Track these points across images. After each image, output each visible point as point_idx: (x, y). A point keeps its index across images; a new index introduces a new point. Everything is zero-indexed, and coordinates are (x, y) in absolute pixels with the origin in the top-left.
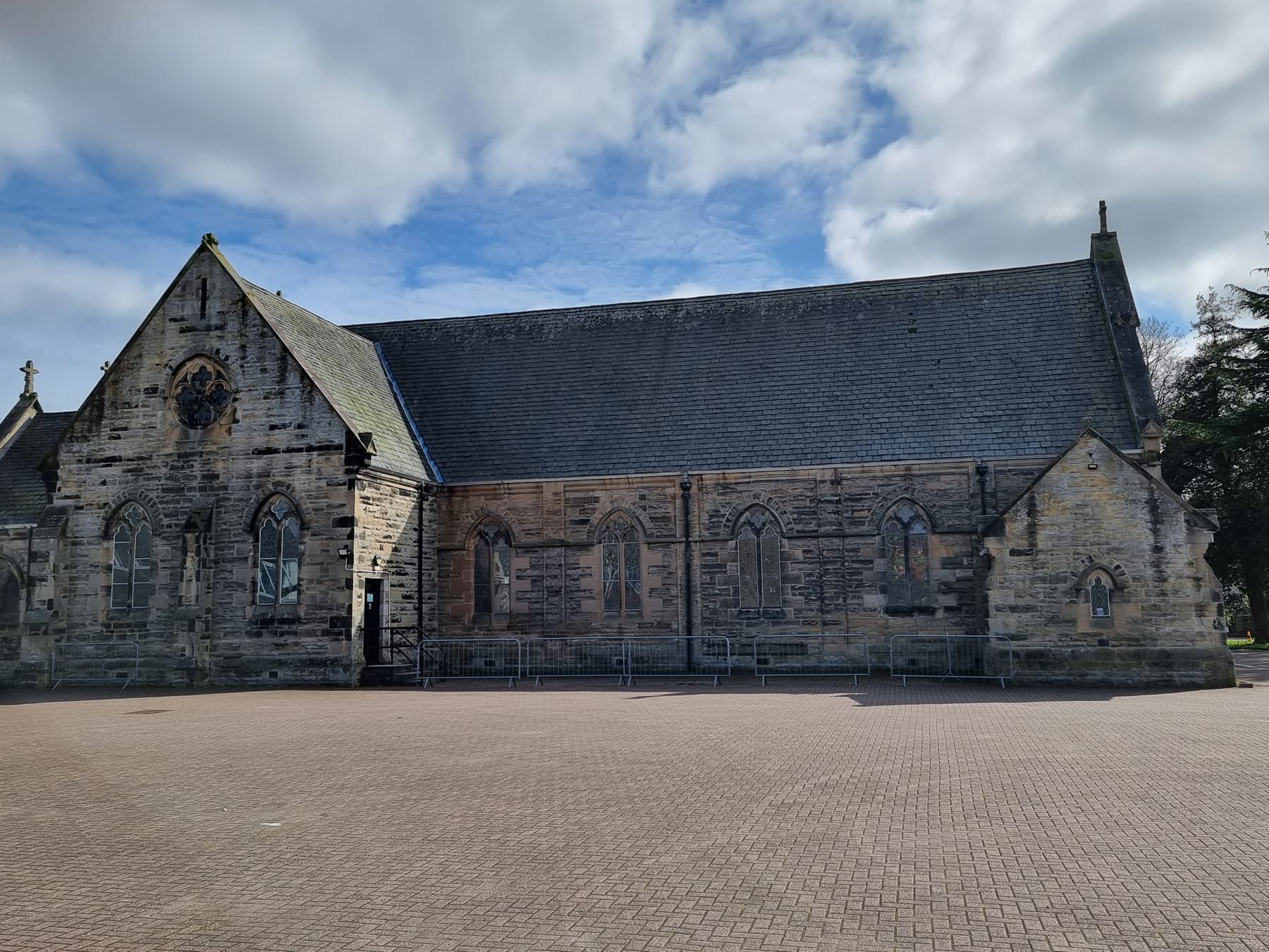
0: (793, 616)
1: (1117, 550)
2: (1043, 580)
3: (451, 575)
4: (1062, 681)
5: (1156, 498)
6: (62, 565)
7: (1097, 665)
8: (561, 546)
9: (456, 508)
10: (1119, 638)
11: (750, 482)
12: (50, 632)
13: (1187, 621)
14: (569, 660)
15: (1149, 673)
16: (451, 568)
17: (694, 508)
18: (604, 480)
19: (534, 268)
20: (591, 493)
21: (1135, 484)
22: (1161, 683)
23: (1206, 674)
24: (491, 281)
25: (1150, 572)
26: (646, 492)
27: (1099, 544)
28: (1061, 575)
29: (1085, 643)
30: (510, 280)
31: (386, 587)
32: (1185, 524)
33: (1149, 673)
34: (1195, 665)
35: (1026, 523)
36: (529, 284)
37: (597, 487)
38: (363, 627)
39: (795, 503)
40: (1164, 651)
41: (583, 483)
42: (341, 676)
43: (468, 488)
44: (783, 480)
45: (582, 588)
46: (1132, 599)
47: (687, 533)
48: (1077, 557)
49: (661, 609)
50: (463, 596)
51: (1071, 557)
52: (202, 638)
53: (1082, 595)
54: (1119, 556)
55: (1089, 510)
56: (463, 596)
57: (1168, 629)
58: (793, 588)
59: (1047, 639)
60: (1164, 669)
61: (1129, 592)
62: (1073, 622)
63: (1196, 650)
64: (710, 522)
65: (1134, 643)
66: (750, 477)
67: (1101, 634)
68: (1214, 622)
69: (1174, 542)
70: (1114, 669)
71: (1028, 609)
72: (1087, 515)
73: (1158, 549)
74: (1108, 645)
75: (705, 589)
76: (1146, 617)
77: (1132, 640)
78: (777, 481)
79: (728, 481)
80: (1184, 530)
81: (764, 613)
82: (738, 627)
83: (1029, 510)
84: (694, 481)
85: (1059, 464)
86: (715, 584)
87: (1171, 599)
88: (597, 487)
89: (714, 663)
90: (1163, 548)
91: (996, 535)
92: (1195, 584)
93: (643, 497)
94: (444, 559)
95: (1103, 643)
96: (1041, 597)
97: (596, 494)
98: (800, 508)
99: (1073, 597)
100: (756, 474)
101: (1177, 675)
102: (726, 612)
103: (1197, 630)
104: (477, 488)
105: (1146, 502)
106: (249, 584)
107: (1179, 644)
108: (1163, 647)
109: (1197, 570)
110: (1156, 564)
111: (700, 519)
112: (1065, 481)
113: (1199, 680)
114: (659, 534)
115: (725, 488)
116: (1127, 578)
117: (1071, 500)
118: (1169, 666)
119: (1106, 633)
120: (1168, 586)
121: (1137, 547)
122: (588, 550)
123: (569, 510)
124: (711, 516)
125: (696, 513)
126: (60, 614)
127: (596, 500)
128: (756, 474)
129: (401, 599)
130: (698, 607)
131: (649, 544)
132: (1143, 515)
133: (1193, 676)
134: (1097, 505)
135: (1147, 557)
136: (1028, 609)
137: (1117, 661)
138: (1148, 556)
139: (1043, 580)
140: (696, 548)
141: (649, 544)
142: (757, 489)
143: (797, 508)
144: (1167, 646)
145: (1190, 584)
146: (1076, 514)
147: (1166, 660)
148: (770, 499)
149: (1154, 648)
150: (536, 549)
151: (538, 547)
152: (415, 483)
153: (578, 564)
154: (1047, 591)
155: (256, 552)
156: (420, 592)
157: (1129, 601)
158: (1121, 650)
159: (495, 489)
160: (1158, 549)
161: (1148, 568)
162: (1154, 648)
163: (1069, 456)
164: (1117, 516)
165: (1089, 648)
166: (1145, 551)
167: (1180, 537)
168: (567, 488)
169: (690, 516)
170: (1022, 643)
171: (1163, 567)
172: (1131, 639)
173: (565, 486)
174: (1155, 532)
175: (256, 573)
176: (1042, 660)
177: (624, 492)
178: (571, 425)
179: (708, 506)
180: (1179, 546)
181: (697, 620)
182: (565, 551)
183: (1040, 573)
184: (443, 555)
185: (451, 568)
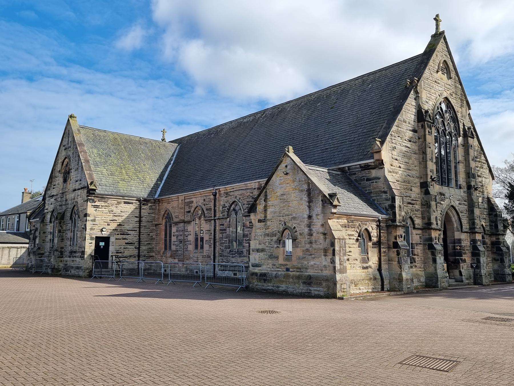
0: (245, 253)
1: (294, 218)
2: (268, 235)
3: (158, 235)
4: (270, 290)
5: (311, 188)
6: (42, 232)
7: (283, 281)
8: (183, 222)
9: (160, 208)
10: (294, 267)
11: (233, 191)
12: (36, 254)
13: (320, 259)
14: (183, 272)
15: (301, 288)
16: (159, 232)
17: (217, 204)
18: (194, 193)
19: (510, 90)
20: (191, 199)
21: (302, 181)
22: (306, 294)
23: (325, 290)
24: (487, 100)
25: (306, 230)
26: (205, 198)
27: (288, 215)
28: (274, 232)
29: (281, 269)
30: (498, 98)
31: (112, 239)
32: (321, 202)
33: (301, 288)
34: (320, 284)
35: (264, 205)
36: (508, 98)
37: (193, 197)
38: (93, 255)
39: (247, 199)
40: (310, 275)
41: (189, 195)
42: (81, 273)
43: (163, 199)
44: (243, 189)
45: (188, 240)
46: (300, 245)
47: (215, 216)
48: (280, 222)
49: (208, 249)
50: (161, 243)
51: (278, 222)
52: (58, 257)
53: (281, 243)
54: (295, 222)
55: (285, 197)
56: (161, 243)
57: (312, 263)
58: (246, 240)
59: (268, 267)
60: (308, 286)
61: (298, 242)
62: (277, 258)
63: (322, 275)
64: (223, 210)
65: (299, 270)
66: (233, 188)
67: (287, 265)
68: (331, 259)
69: (316, 213)
70: (289, 285)
71: (263, 250)
72: (285, 199)
73: (310, 217)
74: (289, 271)
75: (220, 240)
76: (304, 256)
77: (299, 269)
78: (242, 190)
79: (228, 191)
80: (321, 205)
81: (237, 252)
82: (229, 258)
83: (265, 198)
84: (217, 192)
85: (276, 173)
86: (223, 238)
87: (314, 246)
88: (193, 197)
89: (221, 274)
90: (312, 216)
91: (254, 212)
92: (324, 236)
93: (204, 200)
94: (157, 228)
95: (288, 270)
96: (267, 244)
97: (191, 200)
98: (249, 202)
99: (278, 244)
100: (235, 187)
101: (314, 289)
102: (226, 251)
103: (324, 264)
104: (165, 199)
105: (306, 191)
106: (70, 238)
107: (316, 271)
108: (310, 273)
109: (325, 229)
110: (309, 226)
111: (219, 208)
112: (278, 182)
113: (322, 294)
114: (208, 216)
115: (227, 194)
116: (298, 234)
117: (279, 192)
118: (310, 284)
119: (289, 264)
120: (313, 238)
121: (302, 216)
122: (190, 224)
123: (186, 207)
124: (223, 207)
125: (218, 206)
126: (41, 248)
127: (192, 202)
128: (235, 187)
129: (125, 244)
130: (217, 249)
131: (206, 220)
132: (305, 198)
133: (319, 291)
134: (289, 194)
135: (306, 222)
136: (263, 250)
137: (291, 280)
138: (306, 221)
139: (268, 235)
140: (217, 221)
141: (206, 220)
142: (236, 193)
143: (248, 202)
144: (311, 272)
145: (322, 237)
146: (281, 199)
147: (309, 281)
148: (240, 198)
149: (306, 273)
150: (178, 224)
151: (178, 223)
152: (136, 199)
153: (187, 230)
154: (269, 241)
155: (72, 227)
156: (139, 241)
157: (298, 247)
158: (294, 274)
159: (168, 200)
160: (310, 217)
161: (306, 228)
162: (306, 273)
163: (279, 168)
164: (295, 199)
165: (282, 272)
166: (305, 218)
167: (319, 210)
168: (178, 199)
169: (216, 208)
170: (260, 268)
171: (312, 227)
172: (298, 268)
173: (185, 197)
174: (309, 207)
175: (71, 234)
176: (264, 278)
177: (200, 198)
178: (202, 170)
179: (222, 203)
180: (318, 215)
181: (217, 255)
182: (184, 224)
183: (267, 231)
184: (157, 226)
185: (159, 232)
